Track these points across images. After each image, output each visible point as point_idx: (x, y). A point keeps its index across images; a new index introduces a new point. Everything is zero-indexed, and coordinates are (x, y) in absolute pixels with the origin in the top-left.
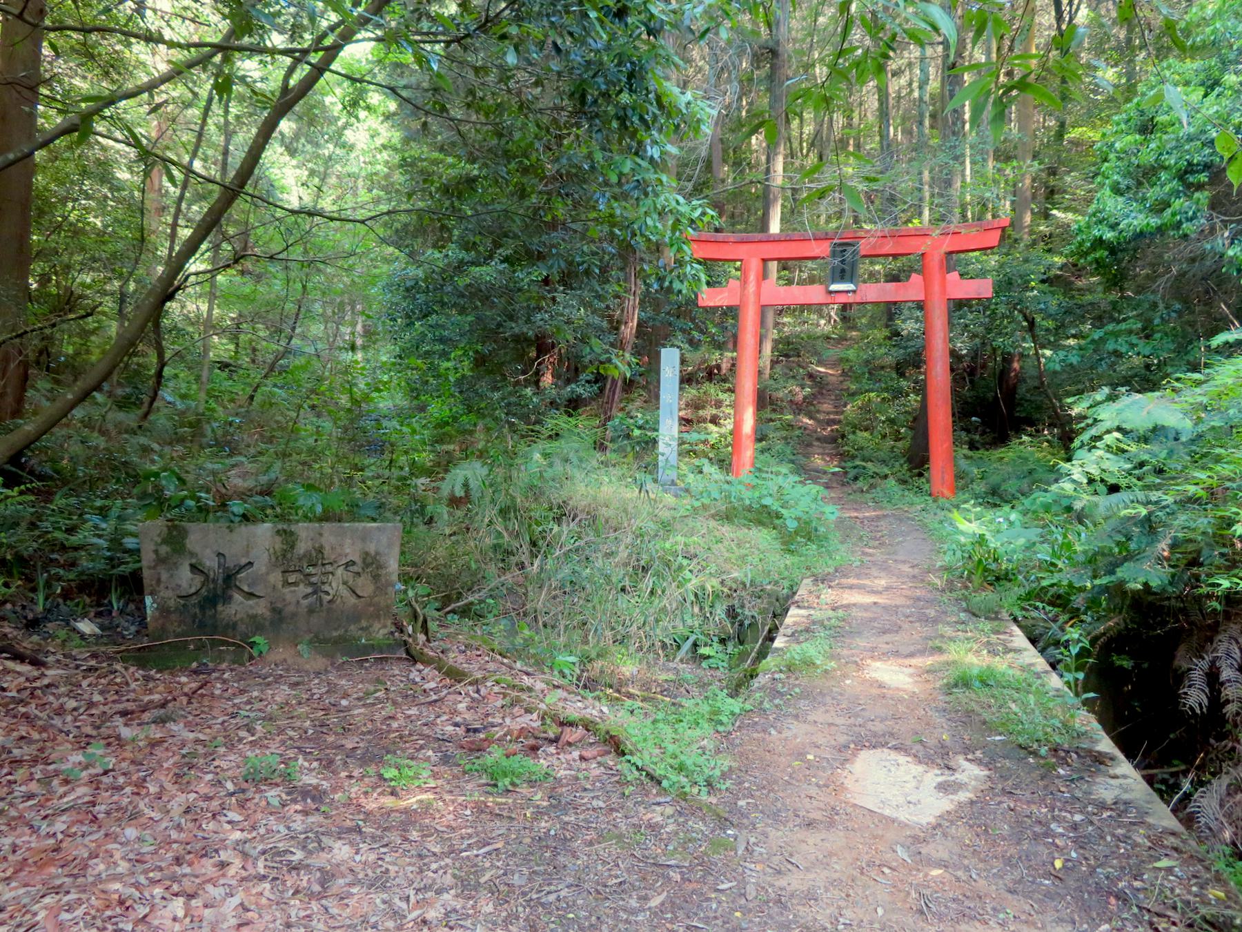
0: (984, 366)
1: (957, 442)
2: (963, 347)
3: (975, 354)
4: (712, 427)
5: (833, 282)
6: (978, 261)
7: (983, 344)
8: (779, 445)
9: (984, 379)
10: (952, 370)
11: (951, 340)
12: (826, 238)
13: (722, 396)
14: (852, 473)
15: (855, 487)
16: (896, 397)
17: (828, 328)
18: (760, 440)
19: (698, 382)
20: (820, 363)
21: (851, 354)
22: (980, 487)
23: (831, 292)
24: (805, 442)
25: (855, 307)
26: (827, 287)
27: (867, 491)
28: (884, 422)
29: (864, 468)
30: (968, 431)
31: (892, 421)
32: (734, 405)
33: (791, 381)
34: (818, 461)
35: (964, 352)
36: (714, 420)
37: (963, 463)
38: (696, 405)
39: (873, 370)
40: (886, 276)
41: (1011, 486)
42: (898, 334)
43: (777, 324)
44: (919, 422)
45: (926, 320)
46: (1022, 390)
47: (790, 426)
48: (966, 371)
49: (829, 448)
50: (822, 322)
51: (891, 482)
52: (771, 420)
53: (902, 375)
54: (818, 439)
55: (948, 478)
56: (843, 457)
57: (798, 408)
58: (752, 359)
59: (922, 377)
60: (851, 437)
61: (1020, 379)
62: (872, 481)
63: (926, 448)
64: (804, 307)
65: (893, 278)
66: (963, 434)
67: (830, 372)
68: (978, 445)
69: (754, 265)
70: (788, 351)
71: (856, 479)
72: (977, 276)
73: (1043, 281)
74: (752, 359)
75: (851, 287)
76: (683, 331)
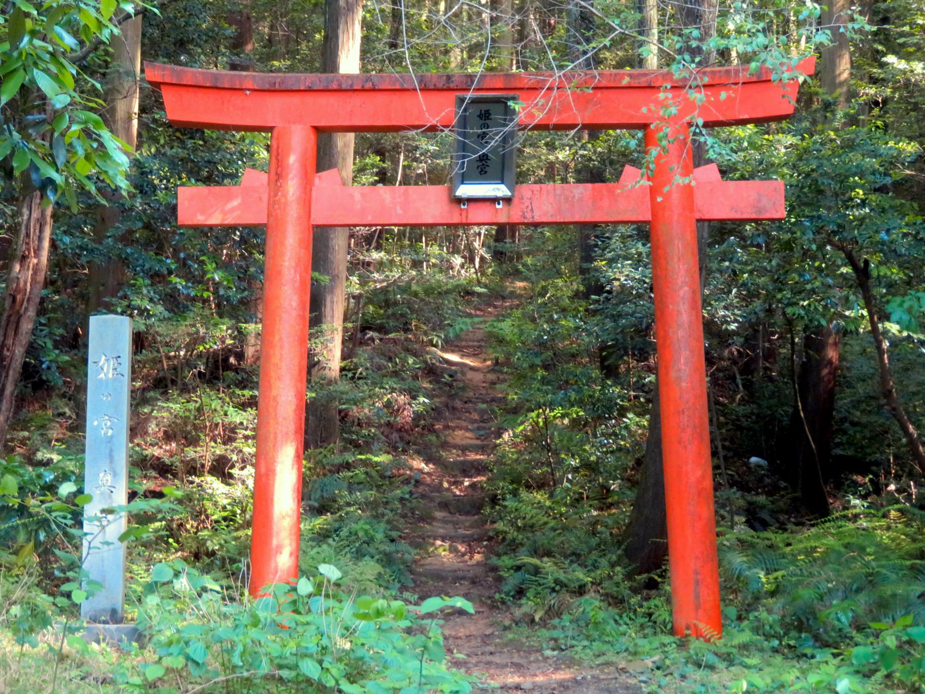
0: (770, 355)
1: (722, 513)
2: (731, 317)
3: (753, 331)
4: (213, 484)
5: (464, 179)
6: (752, 144)
7: (770, 311)
8: (359, 523)
9: (771, 379)
10: (710, 361)
11: (706, 302)
12: (447, 86)
13: (236, 417)
14: (512, 580)
15: (518, 613)
16: (600, 419)
17: (470, 273)
18: (320, 510)
19: (185, 389)
20: (449, 345)
21: (506, 327)
22: (770, 614)
23: (459, 201)
24: (414, 513)
25: (523, 231)
26: (451, 190)
27: (544, 623)
28: (576, 470)
29: (537, 571)
30: (744, 487)
31: (590, 467)
32: (257, 437)
33: (391, 383)
34: (443, 554)
35: (733, 327)
36: (221, 469)
37: (738, 560)
38: (183, 433)
39: (552, 362)
40: (578, 171)
41: (839, 614)
42: (599, 289)
43: (355, 266)
44: (646, 469)
45: (655, 260)
46: (843, 401)
47: (383, 478)
48: (734, 365)
49: (466, 525)
50: (457, 260)
51: (591, 604)
52: (348, 466)
53: (610, 372)
54: (444, 506)
55: (708, 596)
56: (497, 543)
57: (402, 438)
58: (297, 345)
59: (651, 378)
60: (510, 503)
61: (840, 380)
62: (553, 600)
63: (662, 529)
64: (416, 232)
65: (593, 174)
66: (734, 494)
67: (467, 361)
68: (765, 515)
69: (298, 145)
70: (381, 323)
71: (520, 593)
72: (752, 176)
73: (882, 190)
74: (297, 345)
75: (500, 190)
76: (157, 277)
